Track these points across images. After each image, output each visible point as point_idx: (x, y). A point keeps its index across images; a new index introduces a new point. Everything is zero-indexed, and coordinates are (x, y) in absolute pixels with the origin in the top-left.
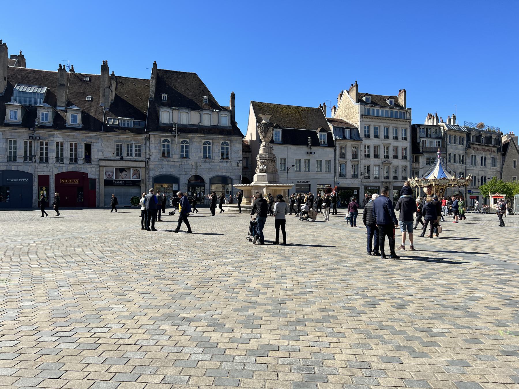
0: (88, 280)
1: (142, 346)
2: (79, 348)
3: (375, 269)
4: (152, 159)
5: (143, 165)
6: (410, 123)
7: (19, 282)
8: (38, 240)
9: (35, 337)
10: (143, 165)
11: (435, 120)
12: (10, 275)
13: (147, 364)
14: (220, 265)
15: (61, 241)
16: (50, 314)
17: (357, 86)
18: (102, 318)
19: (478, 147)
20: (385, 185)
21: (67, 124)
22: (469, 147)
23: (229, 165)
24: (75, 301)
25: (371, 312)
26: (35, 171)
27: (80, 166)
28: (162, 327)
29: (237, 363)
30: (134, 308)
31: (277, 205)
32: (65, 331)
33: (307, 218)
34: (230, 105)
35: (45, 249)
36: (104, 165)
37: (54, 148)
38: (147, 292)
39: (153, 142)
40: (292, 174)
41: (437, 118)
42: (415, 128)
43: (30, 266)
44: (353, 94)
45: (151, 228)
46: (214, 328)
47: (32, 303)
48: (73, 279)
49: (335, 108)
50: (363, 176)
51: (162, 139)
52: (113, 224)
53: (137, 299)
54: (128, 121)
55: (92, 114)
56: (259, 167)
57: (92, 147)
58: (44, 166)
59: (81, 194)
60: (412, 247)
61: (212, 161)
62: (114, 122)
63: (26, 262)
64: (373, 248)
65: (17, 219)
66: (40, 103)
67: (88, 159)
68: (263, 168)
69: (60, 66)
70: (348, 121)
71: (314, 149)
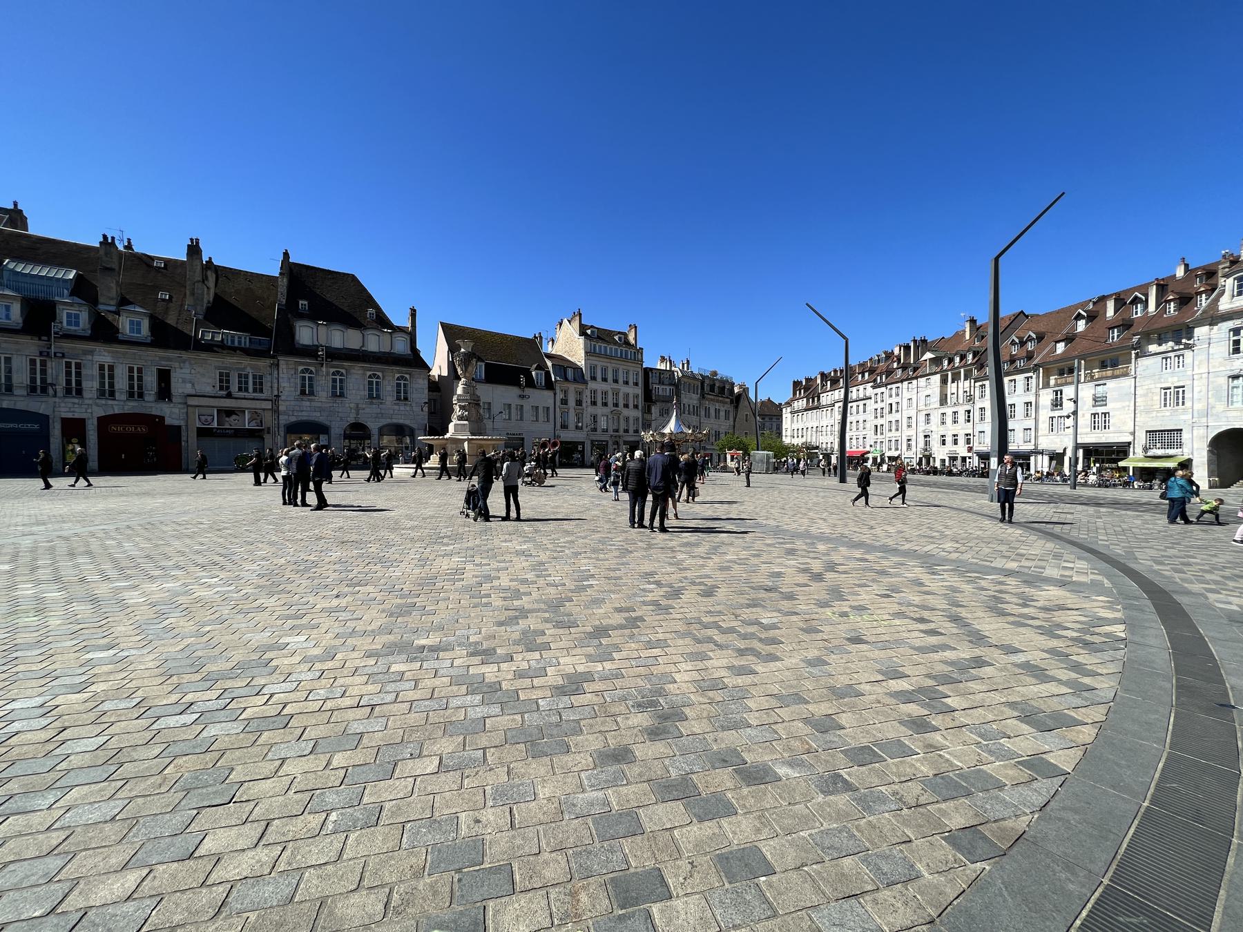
0: (217, 596)
1: (373, 707)
2: (250, 730)
3: (650, 546)
4: (283, 398)
5: (268, 405)
6: (642, 365)
7: (65, 612)
8: (84, 529)
9: (143, 723)
10: (268, 405)
11: (668, 363)
12: (39, 600)
13: (399, 740)
14: (440, 556)
15: (133, 530)
16: (161, 670)
17: (580, 315)
18: (274, 664)
19: (712, 397)
20: (614, 439)
21: (120, 335)
22: (704, 397)
23: (408, 408)
24: (205, 639)
25: (680, 605)
26: (54, 411)
27: (148, 405)
28: (394, 668)
29: (547, 712)
30: (327, 640)
31: (508, 465)
32: (207, 699)
33: (531, 482)
34: (409, 325)
35: (105, 548)
36: (197, 404)
37: (94, 373)
38: (338, 609)
39: (285, 371)
40: (499, 424)
41: (670, 361)
42: (647, 372)
43: (83, 580)
44: (576, 324)
45: (299, 503)
46: (480, 658)
47: (112, 652)
48: (184, 598)
49: (553, 341)
50: (589, 428)
51: (300, 368)
52: (225, 498)
53: (326, 623)
54: (240, 338)
55: (171, 320)
56: (457, 411)
57: (173, 375)
58: (74, 403)
59: (151, 450)
60: (676, 515)
61: (381, 403)
62: (213, 337)
63: (71, 572)
64: (636, 520)
65: (17, 496)
66: (62, 296)
67: (164, 392)
68: (462, 414)
69: (105, 237)
70: (569, 358)
71: (528, 391)
